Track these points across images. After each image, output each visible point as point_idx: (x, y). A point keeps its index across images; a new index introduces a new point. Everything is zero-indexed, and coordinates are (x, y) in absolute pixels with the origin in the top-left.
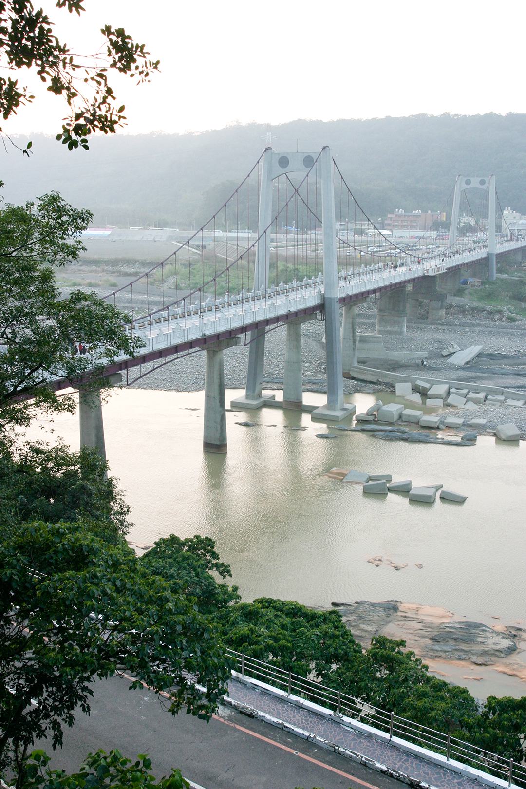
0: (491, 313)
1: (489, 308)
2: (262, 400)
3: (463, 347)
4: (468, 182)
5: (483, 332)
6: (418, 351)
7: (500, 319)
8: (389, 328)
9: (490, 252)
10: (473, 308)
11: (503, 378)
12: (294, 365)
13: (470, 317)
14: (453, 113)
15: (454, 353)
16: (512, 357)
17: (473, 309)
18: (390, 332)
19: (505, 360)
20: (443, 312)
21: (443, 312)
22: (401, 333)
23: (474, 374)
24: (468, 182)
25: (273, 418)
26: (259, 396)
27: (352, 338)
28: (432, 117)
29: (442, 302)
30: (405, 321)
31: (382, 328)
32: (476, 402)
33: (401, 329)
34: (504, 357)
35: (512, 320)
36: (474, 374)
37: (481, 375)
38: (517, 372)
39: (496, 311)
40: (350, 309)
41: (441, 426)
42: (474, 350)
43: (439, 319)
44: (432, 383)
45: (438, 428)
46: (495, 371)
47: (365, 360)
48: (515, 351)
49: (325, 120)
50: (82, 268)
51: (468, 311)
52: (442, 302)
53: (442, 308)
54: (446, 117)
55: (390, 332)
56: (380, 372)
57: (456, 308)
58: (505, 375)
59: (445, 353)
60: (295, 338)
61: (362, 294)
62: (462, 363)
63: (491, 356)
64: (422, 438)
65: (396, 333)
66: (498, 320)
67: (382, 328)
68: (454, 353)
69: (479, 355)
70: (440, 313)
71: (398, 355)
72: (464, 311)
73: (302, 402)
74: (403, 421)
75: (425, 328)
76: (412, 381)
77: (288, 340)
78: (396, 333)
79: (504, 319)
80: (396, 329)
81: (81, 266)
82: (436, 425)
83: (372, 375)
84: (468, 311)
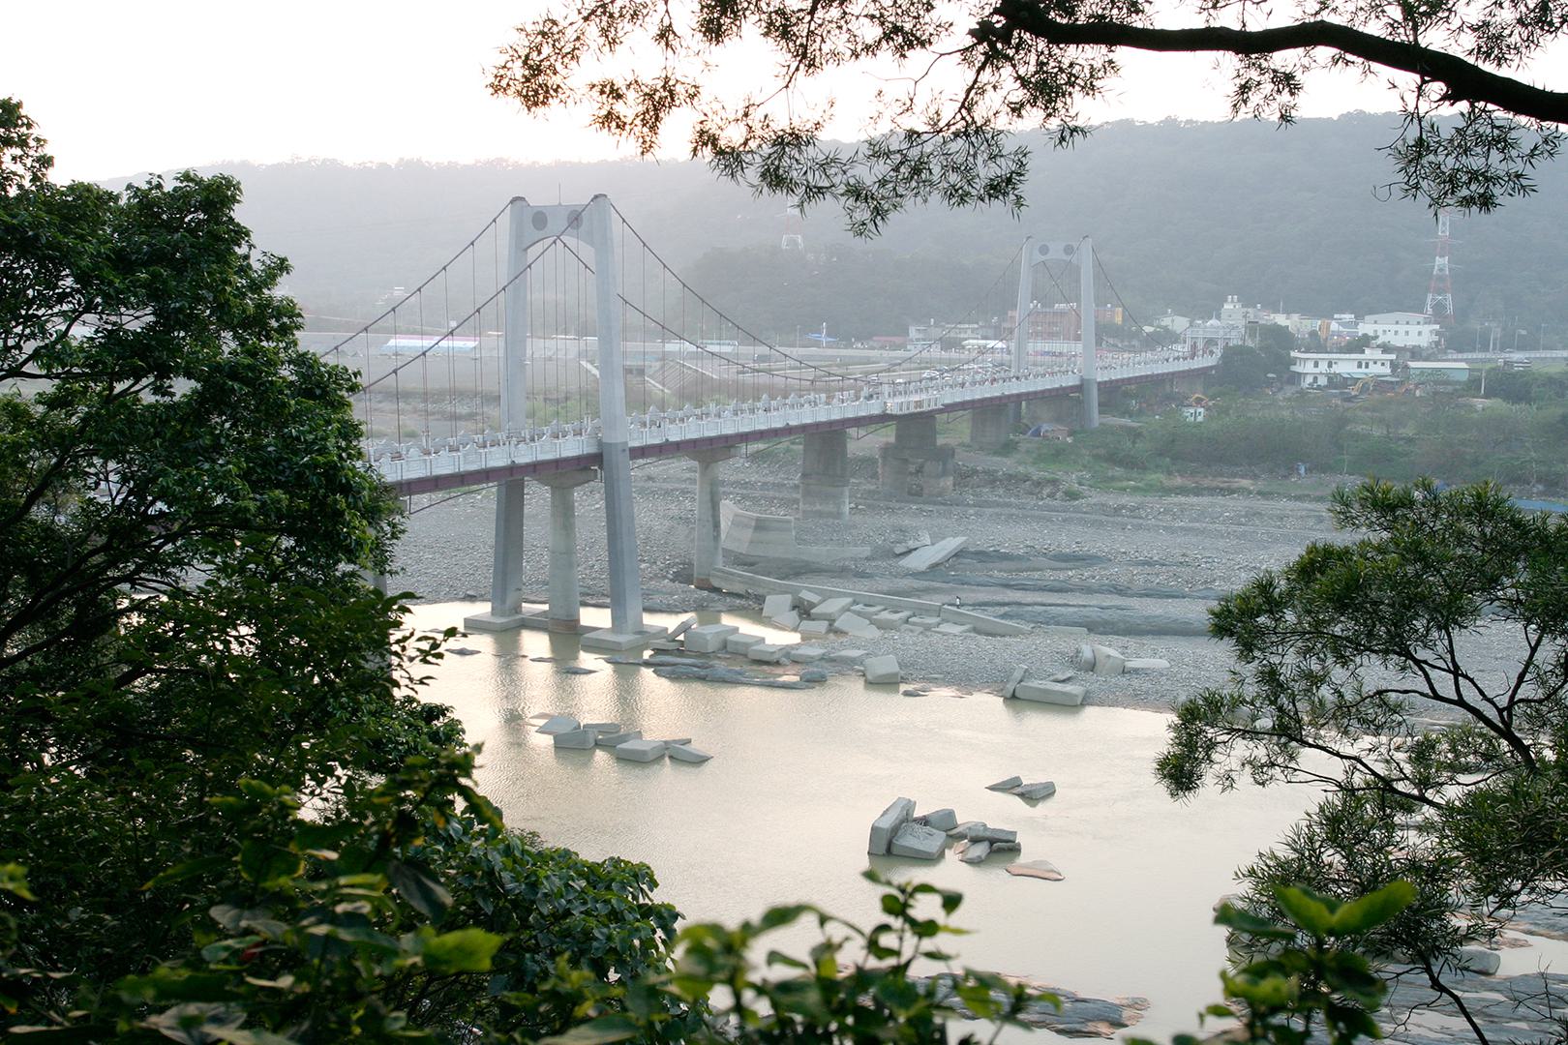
0: (1038, 484)
1: (1036, 474)
2: (520, 616)
3: (936, 538)
4: (1044, 250)
5: (998, 515)
6: (856, 545)
7: (1051, 496)
8: (818, 507)
9: (1085, 377)
10: (1010, 475)
11: (973, 591)
12: (565, 557)
13: (1001, 491)
14: (1183, 117)
15: (915, 549)
16: (1019, 558)
17: (1010, 477)
18: (820, 514)
19: (1005, 563)
20: (949, 481)
21: (949, 481)
22: (839, 515)
23: (926, 584)
24: (1044, 250)
25: (536, 644)
26: (517, 609)
27: (710, 519)
28: (1146, 125)
29: (944, 464)
30: (847, 493)
31: (808, 508)
32: (882, 626)
33: (839, 508)
34: (1006, 557)
35: (1072, 496)
36: (926, 584)
37: (938, 585)
38: (1004, 582)
39: (1049, 481)
40: (707, 468)
41: (784, 660)
42: (952, 544)
43: (940, 494)
44: (826, 596)
45: (777, 663)
46: (966, 580)
47: (752, 560)
48: (1027, 546)
49: (350, 160)
50: (380, 405)
51: (1000, 481)
52: (944, 464)
53: (944, 473)
54: (1170, 123)
55: (820, 514)
56: (751, 578)
57: (981, 476)
58: (982, 585)
59: (899, 549)
60: (564, 512)
61: (726, 438)
62: (923, 567)
63: (982, 556)
64: (728, 676)
65: (830, 515)
66: (1048, 496)
67: (808, 508)
68: (915, 549)
69: (959, 554)
70: (942, 484)
71: (817, 552)
72: (994, 481)
73: (578, 621)
74: (727, 652)
75: (899, 509)
76: (794, 591)
77: (553, 515)
78: (830, 515)
79: (1059, 495)
80: (831, 508)
81: (380, 402)
82: (774, 658)
83: (740, 582)
84: (1000, 481)
